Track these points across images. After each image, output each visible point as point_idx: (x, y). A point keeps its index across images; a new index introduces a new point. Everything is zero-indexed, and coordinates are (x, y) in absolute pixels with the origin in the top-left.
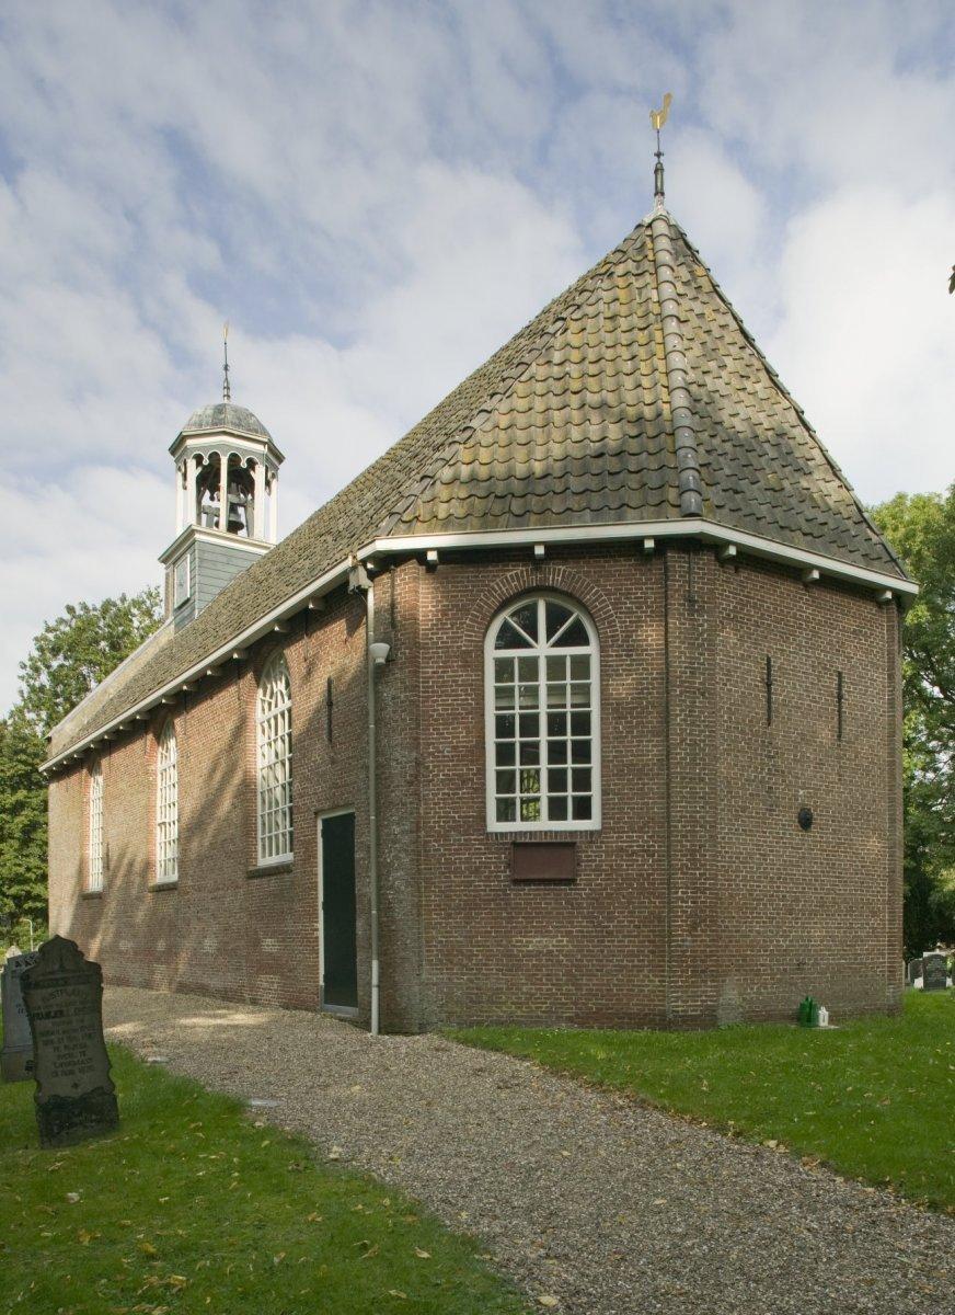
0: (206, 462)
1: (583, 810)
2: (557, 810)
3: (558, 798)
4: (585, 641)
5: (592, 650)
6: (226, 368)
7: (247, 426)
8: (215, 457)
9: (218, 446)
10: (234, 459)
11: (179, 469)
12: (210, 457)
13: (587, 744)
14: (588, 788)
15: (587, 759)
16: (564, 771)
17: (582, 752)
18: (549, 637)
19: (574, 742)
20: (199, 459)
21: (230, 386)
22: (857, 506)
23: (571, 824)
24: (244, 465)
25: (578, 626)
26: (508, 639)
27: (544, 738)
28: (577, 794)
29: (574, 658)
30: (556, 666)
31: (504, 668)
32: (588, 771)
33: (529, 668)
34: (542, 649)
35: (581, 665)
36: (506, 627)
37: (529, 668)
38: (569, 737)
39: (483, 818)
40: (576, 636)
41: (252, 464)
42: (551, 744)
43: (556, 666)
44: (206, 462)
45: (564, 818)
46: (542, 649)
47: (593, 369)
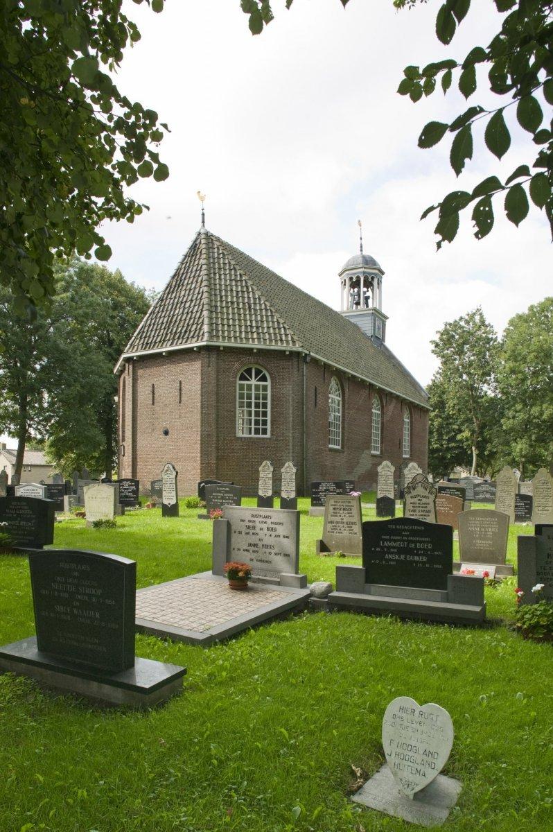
0: (354, 280)
1: (265, 432)
2: (257, 431)
4: (266, 380)
5: (268, 383)
8: (358, 278)
14: (266, 417)
15: (266, 408)
17: (265, 414)
18: (256, 378)
22: (400, 441)
23: (261, 436)
25: (264, 376)
26: (243, 378)
27: (253, 400)
29: (263, 386)
30: (257, 387)
31: (242, 387)
32: (267, 403)
33: (249, 387)
34: (253, 382)
35: (265, 388)
36: (242, 374)
37: (249, 387)
38: (261, 427)
40: (264, 379)
42: (251, 391)
43: (257, 387)
44: (354, 280)
46: (253, 382)
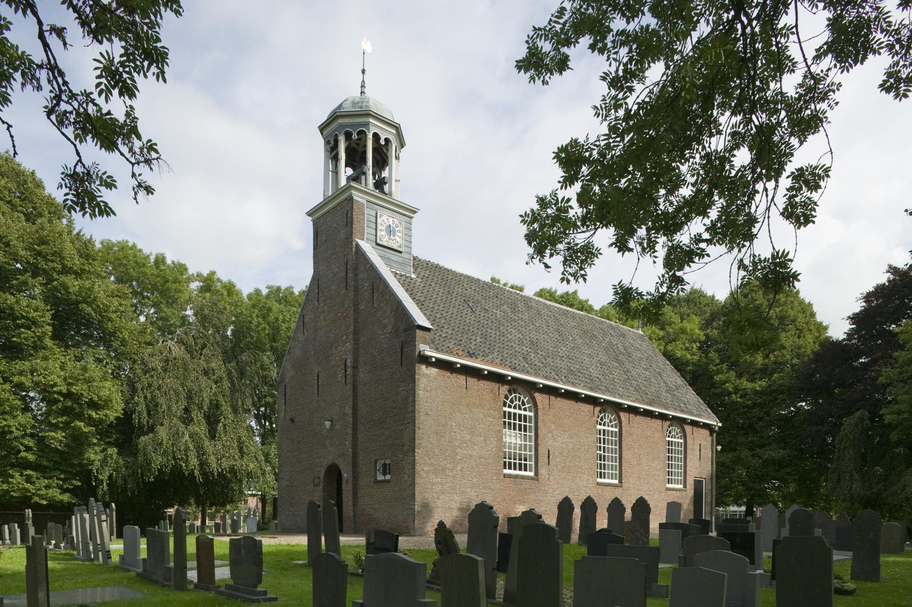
6: (363, 72)
8: (362, 133)
10: (348, 136)
24: (355, 136)
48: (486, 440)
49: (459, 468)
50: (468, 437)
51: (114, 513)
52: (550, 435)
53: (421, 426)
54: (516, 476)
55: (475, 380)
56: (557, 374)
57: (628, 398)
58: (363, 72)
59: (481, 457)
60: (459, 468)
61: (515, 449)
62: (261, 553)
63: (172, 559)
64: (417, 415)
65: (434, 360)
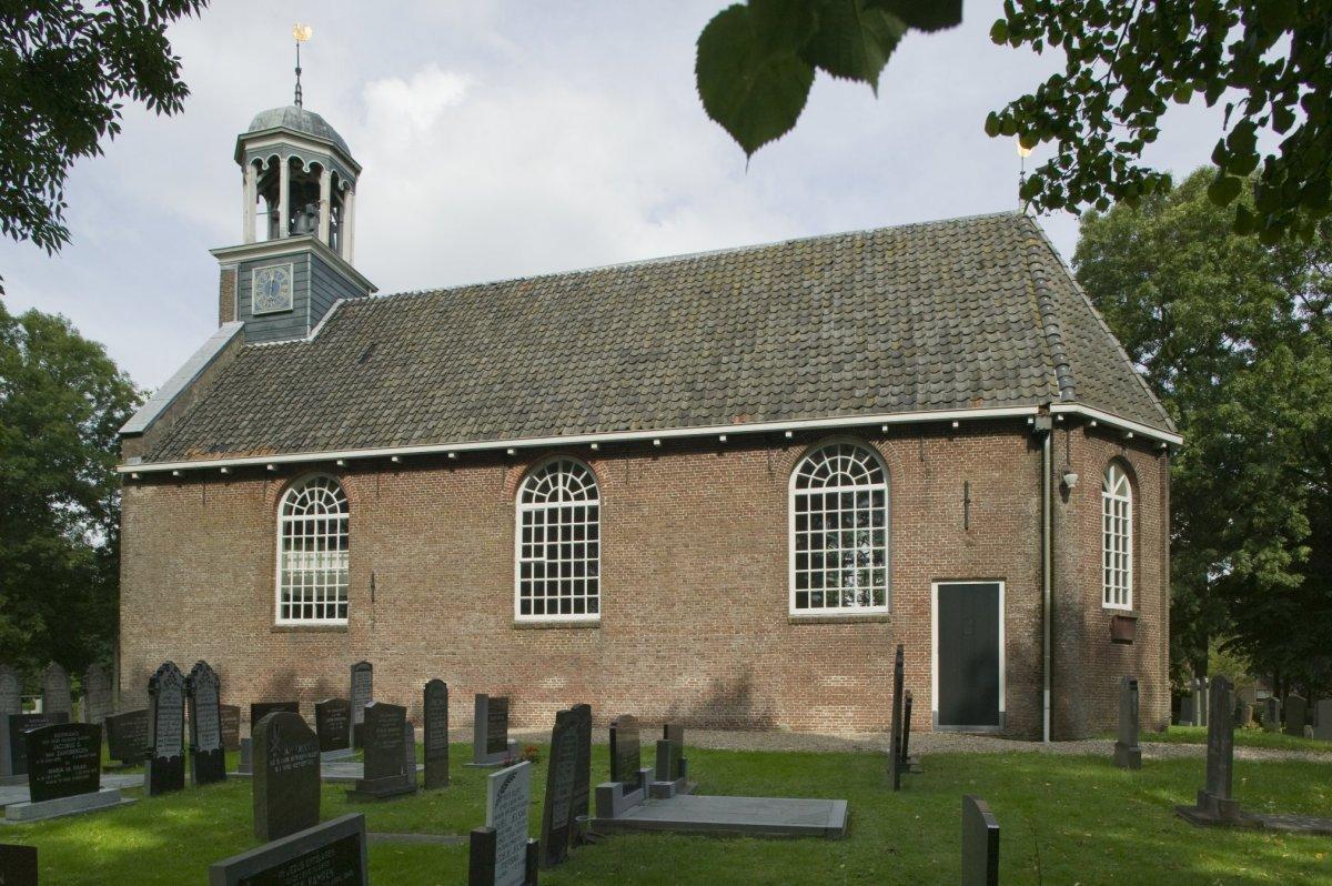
0: (265, 167)
3: (553, 600)
6: (298, 71)
7: (318, 131)
8: (274, 162)
9: (276, 148)
10: (295, 164)
11: (957, 571)
12: (270, 162)
13: (798, 528)
16: (570, 527)
19: (812, 535)
20: (258, 163)
21: (303, 92)
24: (306, 169)
28: (586, 584)
39: (513, 615)
41: (317, 169)
44: (265, 167)
45: (806, 607)
47: (871, 331)
48: (236, 576)
49: (188, 625)
50: (204, 576)
51: (1199, 711)
52: (377, 547)
53: (129, 573)
54: (563, 626)
55: (447, 473)
56: (745, 410)
57: (449, 437)
58: (298, 71)
59: (226, 604)
60: (188, 625)
61: (332, 580)
62: (1232, 761)
63: (420, 755)
64: (123, 558)
65: (956, 425)
